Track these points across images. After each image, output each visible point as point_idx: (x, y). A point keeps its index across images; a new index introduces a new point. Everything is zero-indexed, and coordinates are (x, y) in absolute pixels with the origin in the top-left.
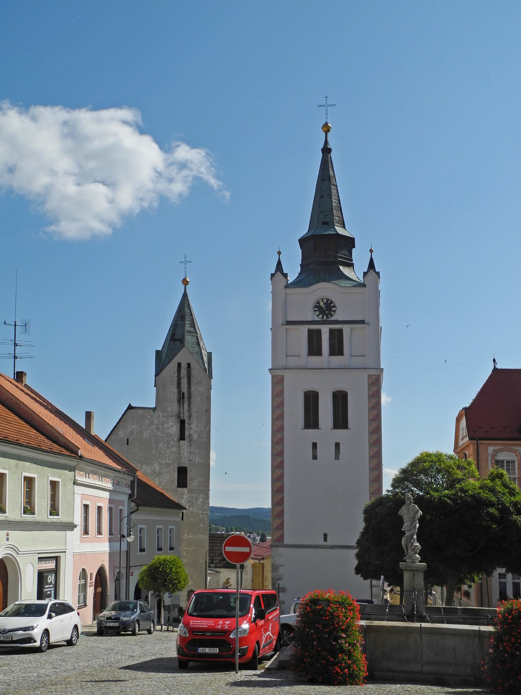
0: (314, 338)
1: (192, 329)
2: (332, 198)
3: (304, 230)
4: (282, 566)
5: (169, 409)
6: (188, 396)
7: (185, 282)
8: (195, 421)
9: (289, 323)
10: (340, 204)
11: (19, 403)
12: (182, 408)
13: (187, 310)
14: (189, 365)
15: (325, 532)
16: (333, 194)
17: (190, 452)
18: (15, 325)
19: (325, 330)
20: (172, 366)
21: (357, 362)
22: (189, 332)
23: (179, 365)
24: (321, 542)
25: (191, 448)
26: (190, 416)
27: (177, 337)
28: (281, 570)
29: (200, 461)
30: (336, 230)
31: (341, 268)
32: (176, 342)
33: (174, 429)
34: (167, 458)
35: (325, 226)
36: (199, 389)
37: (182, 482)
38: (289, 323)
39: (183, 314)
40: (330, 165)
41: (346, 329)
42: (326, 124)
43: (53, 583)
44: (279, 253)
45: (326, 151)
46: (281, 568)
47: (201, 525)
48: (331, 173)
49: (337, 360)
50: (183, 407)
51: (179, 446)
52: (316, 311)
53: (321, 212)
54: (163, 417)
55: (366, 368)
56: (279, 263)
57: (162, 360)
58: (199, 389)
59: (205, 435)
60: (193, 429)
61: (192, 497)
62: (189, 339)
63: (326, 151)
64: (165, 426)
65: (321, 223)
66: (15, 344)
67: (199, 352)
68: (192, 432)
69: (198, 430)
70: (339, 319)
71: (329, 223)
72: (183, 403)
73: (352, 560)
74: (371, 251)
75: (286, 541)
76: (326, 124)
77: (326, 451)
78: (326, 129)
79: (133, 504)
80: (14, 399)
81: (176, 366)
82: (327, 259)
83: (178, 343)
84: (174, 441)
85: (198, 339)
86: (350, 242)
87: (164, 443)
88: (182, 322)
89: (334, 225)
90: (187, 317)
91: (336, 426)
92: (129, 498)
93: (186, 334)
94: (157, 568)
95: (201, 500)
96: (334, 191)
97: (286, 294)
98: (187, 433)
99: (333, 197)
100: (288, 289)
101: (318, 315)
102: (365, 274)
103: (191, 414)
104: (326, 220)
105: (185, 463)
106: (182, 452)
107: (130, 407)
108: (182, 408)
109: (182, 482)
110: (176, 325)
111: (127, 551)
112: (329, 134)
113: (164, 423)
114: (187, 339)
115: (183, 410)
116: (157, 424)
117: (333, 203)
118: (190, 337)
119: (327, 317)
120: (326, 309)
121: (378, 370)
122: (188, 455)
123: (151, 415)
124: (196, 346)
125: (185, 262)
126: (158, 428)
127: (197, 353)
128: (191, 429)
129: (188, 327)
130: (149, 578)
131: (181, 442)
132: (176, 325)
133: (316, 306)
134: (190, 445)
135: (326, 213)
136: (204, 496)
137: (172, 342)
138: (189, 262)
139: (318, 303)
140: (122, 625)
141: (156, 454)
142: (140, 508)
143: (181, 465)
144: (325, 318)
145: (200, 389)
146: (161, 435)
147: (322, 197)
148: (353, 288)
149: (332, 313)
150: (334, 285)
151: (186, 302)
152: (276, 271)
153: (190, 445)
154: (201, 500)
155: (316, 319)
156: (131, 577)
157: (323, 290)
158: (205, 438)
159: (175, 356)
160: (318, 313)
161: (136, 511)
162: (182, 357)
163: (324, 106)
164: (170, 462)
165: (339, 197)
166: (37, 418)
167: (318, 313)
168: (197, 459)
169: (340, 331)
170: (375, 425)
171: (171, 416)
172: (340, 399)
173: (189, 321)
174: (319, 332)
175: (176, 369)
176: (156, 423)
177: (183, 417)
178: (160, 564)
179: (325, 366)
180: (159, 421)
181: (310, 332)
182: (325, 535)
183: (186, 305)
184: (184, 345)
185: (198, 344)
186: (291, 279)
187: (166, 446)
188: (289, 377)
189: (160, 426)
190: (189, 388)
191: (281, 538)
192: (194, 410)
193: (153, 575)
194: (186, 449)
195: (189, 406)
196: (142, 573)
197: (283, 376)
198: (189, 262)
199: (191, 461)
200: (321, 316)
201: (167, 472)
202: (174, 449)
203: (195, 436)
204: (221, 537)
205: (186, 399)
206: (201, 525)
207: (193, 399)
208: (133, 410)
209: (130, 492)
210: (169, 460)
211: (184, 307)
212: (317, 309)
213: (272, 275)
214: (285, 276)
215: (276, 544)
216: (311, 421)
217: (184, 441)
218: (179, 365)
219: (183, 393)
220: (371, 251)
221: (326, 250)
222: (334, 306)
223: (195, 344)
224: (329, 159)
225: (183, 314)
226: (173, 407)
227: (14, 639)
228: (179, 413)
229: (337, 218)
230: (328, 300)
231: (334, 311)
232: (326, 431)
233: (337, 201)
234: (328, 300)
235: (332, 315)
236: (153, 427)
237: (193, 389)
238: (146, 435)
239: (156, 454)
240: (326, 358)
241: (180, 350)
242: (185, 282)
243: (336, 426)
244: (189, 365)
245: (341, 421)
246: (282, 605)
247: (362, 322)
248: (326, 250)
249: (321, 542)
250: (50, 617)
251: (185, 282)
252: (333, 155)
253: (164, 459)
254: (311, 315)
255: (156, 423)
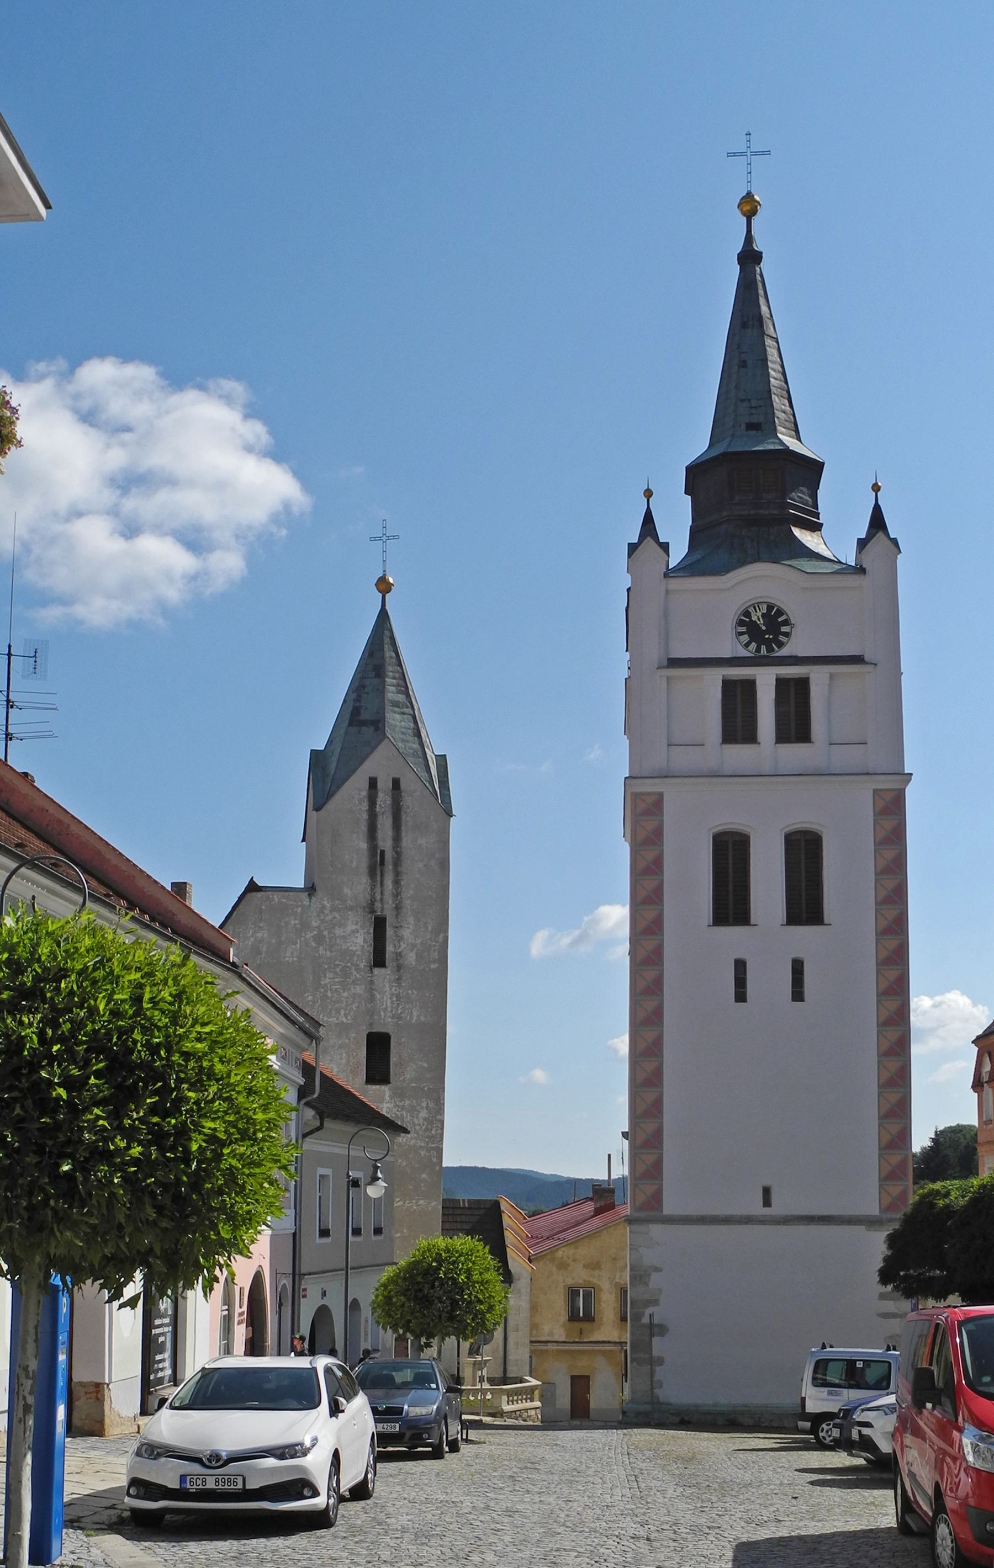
0: (738, 699)
1: (401, 698)
2: (767, 367)
3: (697, 443)
4: (658, 1270)
5: (347, 891)
6: (393, 857)
7: (382, 587)
8: (411, 920)
9: (674, 663)
10: (786, 383)
11: (67, 820)
12: (378, 890)
13: (389, 653)
14: (396, 783)
15: (767, 1183)
16: (770, 358)
17: (398, 996)
18: (9, 655)
19: (766, 681)
20: (355, 787)
21: (844, 758)
22: (396, 704)
23: (373, 783)
24: (758, 1209)
25: (400, 985)
26: (398, 908)
27: (365, 716)
28: (655, 1280)
29: (422, 1018)
30: (781, 442)
31: (797, 532)
32: (364, 729)
33: (359, 940)
34: (342, 1012)
35: (753, 432)
36: (420, 841)
37: (378, 1071)
38: (674, 663)
39: (380, 658)
40: (761, 292)
41: (818, 677)
42: (749, 197)
43: (170, 1312)
44: (648, 494)
45: (749, 258)
46: (654, 1277)
47: (424, 1176)
48: (764, 309)
49: (794, 753)
50: (382, 885)
51: (372, 982)
52: (741, 634)
53: (743, 401)
54: (334, 909)
55: (868, 774)
56: (648, 519)
57: (325, 774)
58: (420, 841)
59: (435, 955)
60: (406, 939)
61: (403, 1108)
62: (395, 720)
63: (749, 258)
64: (338, 931)
65: (743, 426)
66: (8, 701)
67: (420, 753)
68: (403, 946)
69: (419, 941)
70: (801, 654)
71: (763, 424)
72: (382, 876)
73: (875, 1247)
74: (876, 488)
75: (670, 1207)
76: (749, 197)
77: (770, 982)
78: (749, 207)
79: (310, 1113)
80: (51, 811)
81: (366, 785)
82: (761, 512)
83: (368, 731)
84: (358, 970)
85: (416, 722)
86: (813, 469)
87: (336, 973)
88: (376, 681)
89: (775, 430)
90: (390, 669)
91: (794, 918)
92: (300, 1098)
93: (388, 708)
94: (429, 1273)
95: (424, 1114)
96: (772, 353)
97: (667, 592)
98: (390, 948)
99: (770, 364)
100: (671, 581)
101: (747, 645)
102: (862, 544)
103: (400, 902)
104: (755, 419)
105: (385, 1024)
106: (378, 996)
107: (252, 887)
108: (378, 890)
109: (378, 1071)
110: (364, 687)
111: (294, 1234)
112: (755, 221)
113: (334, 926)
114: (392, 722)
115: (382, 894)
116: (318, 927)
117: (772, 380)
118: (398, 716)
119: (770, 649)
120: (766, 629)
121: (900, 777)
122: (392, 1002)
123: (302, 906)
124: (411, 739)
125: (384, 538)
126: (319, 939)
127: (415, 754)
128: (400, 939)
129: (392, 693)
130: (409, 1300)
131: (377, 971)
132: (364, 687)
133: (740, 623)
134: (399, 979)
135: (754, 403)
136: (431, 1105)
137: (354, 729)
138: (395, 537)
139: (747, 614)
140: (410, 1428)
141: (314, 1002)
142: (328, 1124)
143: (376, 1029)
144: (763, 648)
145: (422, 841)
146: (328, 953)
147: (743, 364)
148: (840, 577)
149: (782, 638)
150: (787, 569)
151: (387, 633)
152: (642, 537)
153: (399, 979)
154: (424, 1114)
155: (743, 653)
156: (302, 1300)
157: (758, 582)
158: (434, 962)
159: (361, 763)
160: (745, 638)
161: (318, 1129)
162: (379, 764)
163: (742, 154)
164: (349, 1020)
165: (783, 366)
166: (114, 861)
167: (745, 638)
168: (415, 1014)
169: (803, 685)
170: (891, 913)
171: (351, 908)
172: (804, 851)
173: (394, 678)
174: (749, 686)
175: (364, 793)
176: (314, 924)
177: (382, 909)
178: (439, 1259)
179: (767, 768)
180: (323, 921)
181: (728, 685)
182: (767, 1192)
183: (387, 640)
184: (385, 734)
185: (418, 734)
186: (674, 561)
187: (340, 983)
188: (675, 797)
189: (326, 933)
190: (397, 839)
191: (656, 1199)
192: (408, 892)
193: (421, 1290)
194: (387, 988)
195: (397, 882)
196: (385, 1286)
197: (661, 795)
198: (395, 537)
199: (399, 1018)
200: (753, 646)
201: (341, 1047)
202: (359, 990)
203: (411, 958)
204: (453, 1208)
205: (389, 867)
206: (424, 1176)
207: (406, 866)
208: (259, 894)
209: (301, 1081)
210: (346, 1015)
211: (382, 644)
212: (744, 629)
213: (632, 548)
214: (665, 547)
215: (642, 1214)
216: (731, 905)
217: (383, 970)
218: (373, 783)
219: (383, 852)
220: (876, 488)
221: (751, 489)
222: (786, 622)
223: (410, 732)
224: (758, 277)
225: (380, 658)
226: (357, 887)
227: (253, 1485)
228: (372, 902)
229: (782, 415)
230: (770, 607)
231: (787, 635)
232: (768, 931)
233: (780, 376)
234: (770, 607)
235: (781, 645)
236: (309, 935)
237: (406, 841)
238: (290, 955)
239: (314, 1002)
240: (768, 747)
241: (374, 748)
242: (382, 587)
243: (794, 918)
244: (396, 783)
245: (805, 905)
246: (658, 1369)
247: (857, 660)
248: (751, 489)
249: (758, 1209)
250: (335, 1410)
251: (384, 586)
252: (766, 267)
253: (333, 1012)
254: (729, 644)
255: (314, 924)
